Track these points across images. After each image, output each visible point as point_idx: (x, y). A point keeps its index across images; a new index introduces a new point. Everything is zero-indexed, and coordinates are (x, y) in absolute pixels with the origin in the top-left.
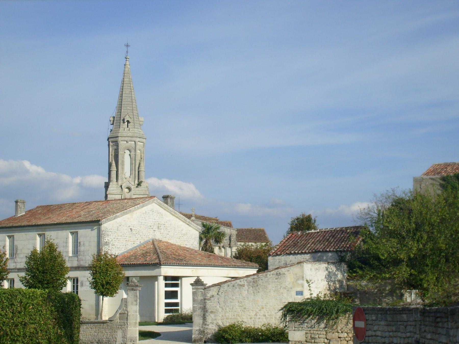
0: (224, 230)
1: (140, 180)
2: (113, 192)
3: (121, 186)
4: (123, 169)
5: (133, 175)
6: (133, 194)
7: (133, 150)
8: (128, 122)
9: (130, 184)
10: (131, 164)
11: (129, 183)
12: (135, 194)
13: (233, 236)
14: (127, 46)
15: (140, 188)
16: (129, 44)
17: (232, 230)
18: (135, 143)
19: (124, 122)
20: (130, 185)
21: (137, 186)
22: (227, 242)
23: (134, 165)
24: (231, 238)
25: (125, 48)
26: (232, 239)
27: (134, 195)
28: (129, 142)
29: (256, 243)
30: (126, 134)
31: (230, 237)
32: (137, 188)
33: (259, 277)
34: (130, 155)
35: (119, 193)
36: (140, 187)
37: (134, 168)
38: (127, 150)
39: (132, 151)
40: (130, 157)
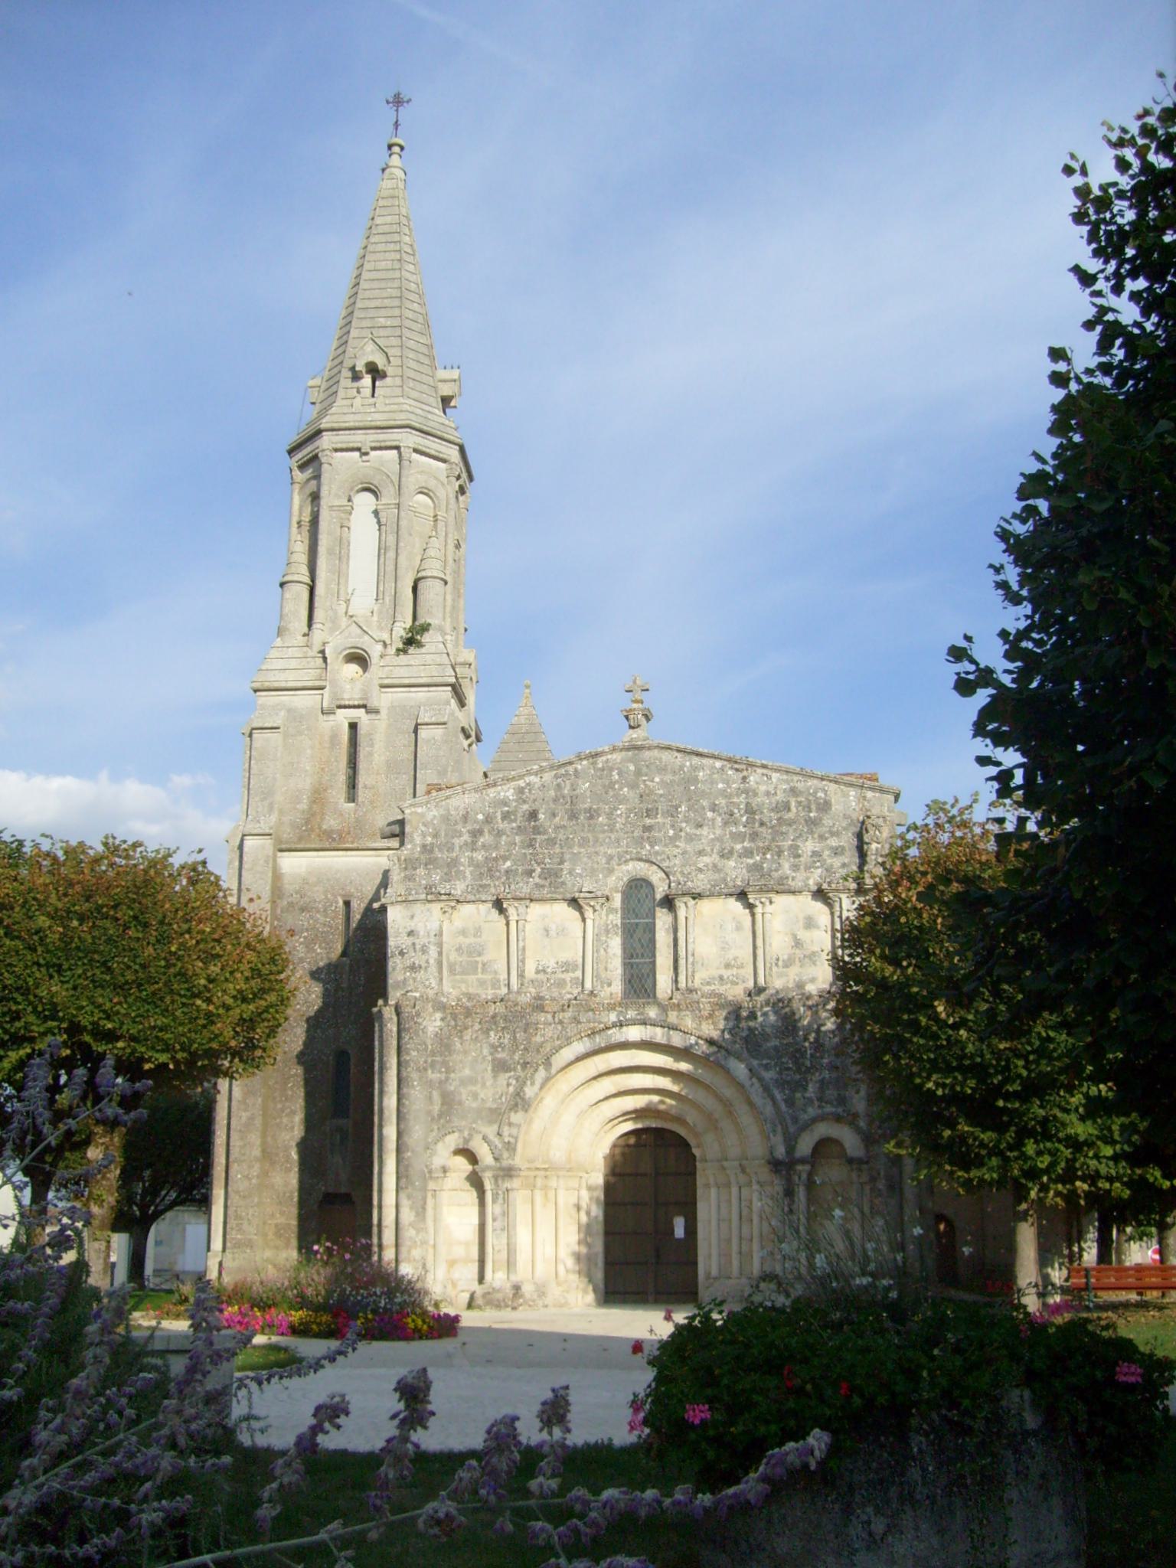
0: (820, 794)
1: (420, 621)
2: (282, 676)
3: (323, 652)
4: (340, 574)
5: (387, 599)
6: (377, 682)
7: (392, 489)
8: (375, 372)
9: (366, 637)
10: (382, 550)
11: (359, 631)
12: (386, 682)
13: (877, 827)
14: (398, 101)
15: (415, 655)
16: (405, 96)
17: (869, 794)
18: (400, 454)
19: (356, 377)
20: (365, 642)
21: (401, 646)
22: (844, 865)
23: (391, 554)
24: (866, 838)
25: (390, 113)
26: (874, 846)
27: (383, 686)
28: (373, 453)
29: (563, 1525)
30: (358, 417)
31: (859, 836)
32: (402, 657)
33: (529, 1161)
34: (376, 513)
35: (310, 684)
36: (418, 651)
37: (390, 567)
38: (359, 491)
39: (384, 492)
40: (379, 522)
